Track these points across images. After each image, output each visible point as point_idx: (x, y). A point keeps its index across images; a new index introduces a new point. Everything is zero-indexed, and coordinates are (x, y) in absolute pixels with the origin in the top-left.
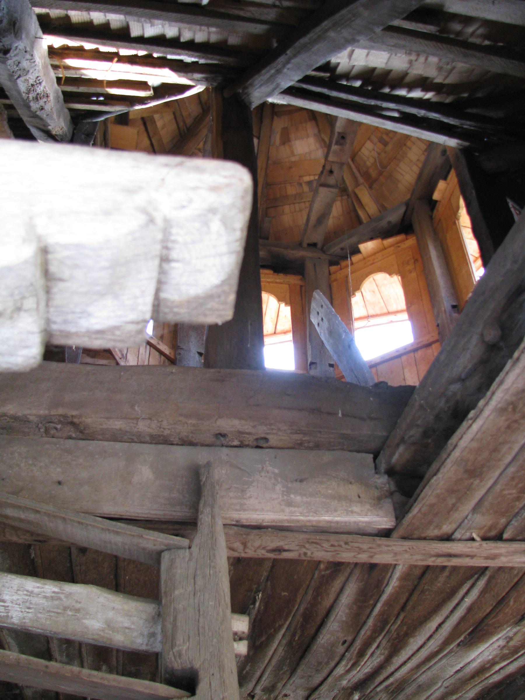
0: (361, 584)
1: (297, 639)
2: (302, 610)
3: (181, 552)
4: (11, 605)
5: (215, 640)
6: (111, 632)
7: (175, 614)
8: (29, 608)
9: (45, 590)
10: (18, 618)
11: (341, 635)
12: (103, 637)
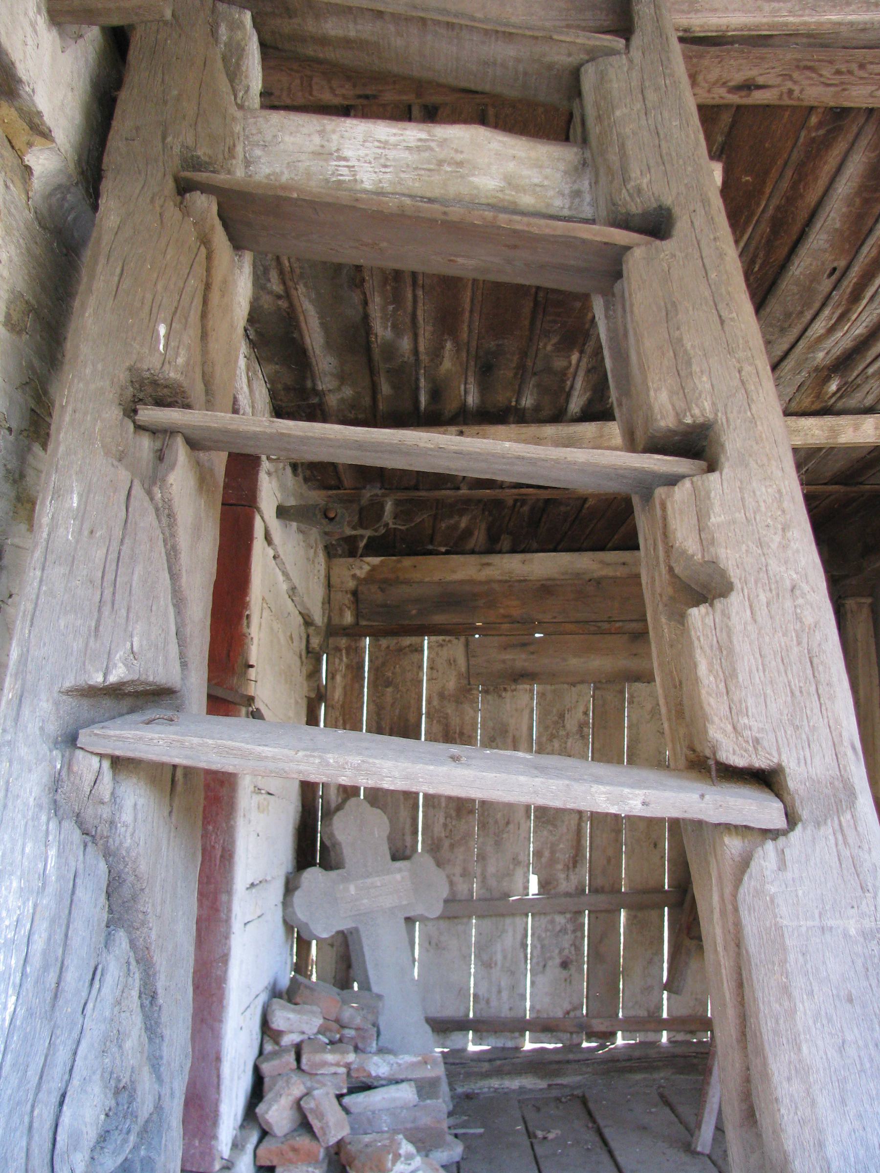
0: (873, 155)
1: (756, 269)
2: (771, 211)
3: (613, 59)
4: (356, 163)
5: (690, 169)
6: (513, 193)
7: (620, 140)
8: (385, 166)
9: (405, 138)
10: (371, 182)
11: (828, 257)
12: (503, 200)
